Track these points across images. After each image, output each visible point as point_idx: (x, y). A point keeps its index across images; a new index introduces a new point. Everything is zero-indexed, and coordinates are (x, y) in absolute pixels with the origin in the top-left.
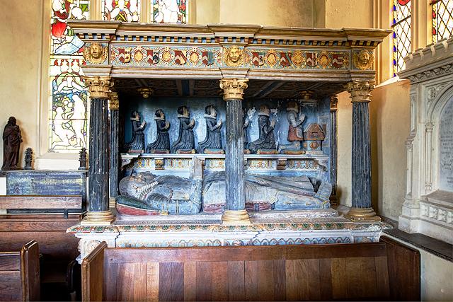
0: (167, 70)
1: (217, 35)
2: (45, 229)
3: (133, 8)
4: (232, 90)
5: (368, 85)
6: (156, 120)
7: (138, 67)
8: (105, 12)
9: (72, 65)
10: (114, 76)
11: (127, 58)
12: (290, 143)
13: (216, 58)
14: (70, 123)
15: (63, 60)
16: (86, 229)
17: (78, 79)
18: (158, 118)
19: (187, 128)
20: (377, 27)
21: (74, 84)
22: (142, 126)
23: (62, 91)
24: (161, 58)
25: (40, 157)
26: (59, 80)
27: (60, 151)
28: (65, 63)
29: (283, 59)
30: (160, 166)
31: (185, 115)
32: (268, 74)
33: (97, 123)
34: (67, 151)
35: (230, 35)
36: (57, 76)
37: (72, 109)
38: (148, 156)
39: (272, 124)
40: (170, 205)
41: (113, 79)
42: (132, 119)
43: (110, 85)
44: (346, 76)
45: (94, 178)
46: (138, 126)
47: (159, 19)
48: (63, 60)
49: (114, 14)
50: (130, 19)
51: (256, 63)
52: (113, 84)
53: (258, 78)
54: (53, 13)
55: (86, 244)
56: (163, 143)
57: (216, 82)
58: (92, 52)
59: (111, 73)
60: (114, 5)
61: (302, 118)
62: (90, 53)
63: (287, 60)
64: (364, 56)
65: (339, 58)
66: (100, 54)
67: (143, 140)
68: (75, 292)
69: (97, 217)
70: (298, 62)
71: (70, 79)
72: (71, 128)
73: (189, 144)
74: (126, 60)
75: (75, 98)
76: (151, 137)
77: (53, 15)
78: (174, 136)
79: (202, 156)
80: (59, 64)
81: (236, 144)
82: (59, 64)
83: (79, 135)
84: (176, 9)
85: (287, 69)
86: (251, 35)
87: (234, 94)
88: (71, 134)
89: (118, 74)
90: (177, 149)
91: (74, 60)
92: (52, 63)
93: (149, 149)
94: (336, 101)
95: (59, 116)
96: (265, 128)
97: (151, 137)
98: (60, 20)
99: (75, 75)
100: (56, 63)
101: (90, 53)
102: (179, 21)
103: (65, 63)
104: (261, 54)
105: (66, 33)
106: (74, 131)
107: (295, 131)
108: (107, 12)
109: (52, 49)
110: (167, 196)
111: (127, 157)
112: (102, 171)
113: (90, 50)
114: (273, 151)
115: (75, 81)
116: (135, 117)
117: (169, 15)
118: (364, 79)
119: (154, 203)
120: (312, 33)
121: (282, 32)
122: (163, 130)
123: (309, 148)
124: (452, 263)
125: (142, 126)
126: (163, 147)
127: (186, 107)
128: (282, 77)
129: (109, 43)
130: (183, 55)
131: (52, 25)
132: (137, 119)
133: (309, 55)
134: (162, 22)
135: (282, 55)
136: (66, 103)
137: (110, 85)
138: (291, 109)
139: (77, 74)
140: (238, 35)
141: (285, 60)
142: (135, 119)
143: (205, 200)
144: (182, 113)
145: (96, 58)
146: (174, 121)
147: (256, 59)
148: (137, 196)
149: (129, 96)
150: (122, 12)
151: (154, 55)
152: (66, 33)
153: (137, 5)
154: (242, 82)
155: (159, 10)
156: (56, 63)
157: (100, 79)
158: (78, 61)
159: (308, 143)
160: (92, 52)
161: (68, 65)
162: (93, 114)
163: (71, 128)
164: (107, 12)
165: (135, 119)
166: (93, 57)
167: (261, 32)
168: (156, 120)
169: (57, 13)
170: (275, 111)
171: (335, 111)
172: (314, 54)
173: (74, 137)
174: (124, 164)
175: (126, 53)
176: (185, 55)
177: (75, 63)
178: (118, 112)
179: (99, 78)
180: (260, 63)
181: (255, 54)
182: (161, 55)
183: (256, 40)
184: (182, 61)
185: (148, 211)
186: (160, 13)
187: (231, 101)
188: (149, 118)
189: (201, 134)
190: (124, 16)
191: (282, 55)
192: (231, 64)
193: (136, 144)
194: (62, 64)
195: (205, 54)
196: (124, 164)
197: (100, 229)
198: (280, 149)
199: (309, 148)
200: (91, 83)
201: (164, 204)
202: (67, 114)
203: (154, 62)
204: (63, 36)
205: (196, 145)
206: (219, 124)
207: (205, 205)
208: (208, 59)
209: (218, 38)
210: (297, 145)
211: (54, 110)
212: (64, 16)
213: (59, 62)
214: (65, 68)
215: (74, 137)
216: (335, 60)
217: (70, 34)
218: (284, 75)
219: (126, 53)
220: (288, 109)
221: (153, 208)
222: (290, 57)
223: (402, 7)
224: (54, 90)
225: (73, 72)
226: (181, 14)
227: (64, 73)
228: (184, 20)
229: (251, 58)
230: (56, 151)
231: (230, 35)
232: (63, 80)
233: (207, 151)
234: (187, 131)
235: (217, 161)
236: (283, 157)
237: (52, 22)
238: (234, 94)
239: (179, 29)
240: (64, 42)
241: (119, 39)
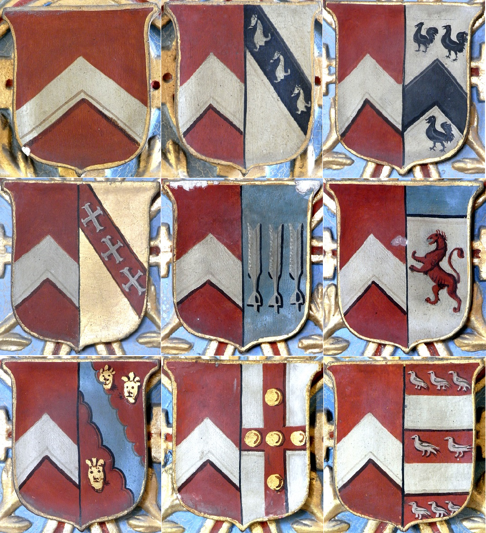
29: (49, 440)
130: (107, 234)
141: (66, 455)
151: (417, 63)
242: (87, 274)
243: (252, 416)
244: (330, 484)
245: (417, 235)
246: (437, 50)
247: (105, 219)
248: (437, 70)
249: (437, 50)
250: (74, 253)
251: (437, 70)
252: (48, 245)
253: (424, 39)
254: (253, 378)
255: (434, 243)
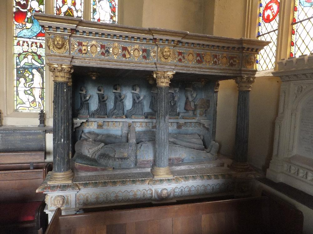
0: (115, 60)
1: (155, 37)
2: (15, 179)
3: (78, 6)
4: (163, 80)
5: (252, 79)
6: (98, 94)
7: (91, 55)
8: (57, 7)
9: (32, 46)
10: (73, 64)
11: (85, 50)
12: (185, 111)
13: (152, 54)
14: (31, 90)
15: (24, 42)
16: (53, 188)
17: (36, 58)
18: (99, 92)
19: (119, 100)
20: (247, 37)
21: (34, 62)
22: (88, 98)
23: (24, 66)
24: (111, 51)
25: (8, 116)
26: (22, 56)
27: (24, 111)
28: (25, 44)
29: (198, 58)
30: (100, 126)
31: (118, 91)
32: (188, 69)
33: (60, 103)
34: (29, 111)
35: (164, 38)
36: (20, 54)
37: (32, 80)
38: (92, 120)
39: (176, 99)
40: (115, 163)
41: (74, 67)
42: (81, 92)
43: (70, 71)
44: (238, 72)
45: (58, 147)
46: (85, 98)
47: (97, 17)
48: (24, 42)
49: (64, 9)
50: (75, 14)
51: (180, 60)
52: (72, 71)
53: (181, 71)
54: (15, 3)
55: (53, 199)
56: (103, 112)
57: (150, 73)
58: (56, 43)
59: (71, 62)
60: (64, 2)
61: (194, 95)
62: (54, 44)
63: (200, 59)
64: (251, 59)
65: (234, 59)
66: (63, 45)
67: (88, 108)
68: (41, 229)
69: (60, 177)
70: (208, 60)
71: (30, 57)
72: (31, 94)
73: (121, 111)
74: (83, 52)
75: (34, 71)
76: (94, 105)
77: (15, 5)
78: (110, 105)
79: (129, 121)
80: (21, 45)
81: (165, 120)
82: (21, 45)
83: (38, 100)
84: (109, 10)
85: (200, 65)
86: (180, 39)
87: (164, 83)
88: (31, 99)
89: (77, 63)
90: (113, 114)
91: (33, 43)
92: (15, 44)
93: (93, 115)
94: (218, 85)
95: (22, 85)
96: (172, 102)
97: (94, 105)
98: (21, 10)
99: (34, 54)
100: (18, 44)
101: (54, 44)
102: (111, 20)
103: (25, 44)
104: (183, 53)
105: (26, 20)
106: (34, 96)
107: (190, 103)
108: (58, 7)
109: (16, 32)
110: (112, 155)
111: (78, 121)
112: (64, 141)
113: (54, 42)
114: (177, 117)
115: (34, 59)
116: (82, 91)
117: (104, 14)
118: (249, 75)
119: (103, 162)
120: (202, 38)
121: (177, 35)
122: (102, 100)
123: (198, 115)
124: (312, 210)
125: (88, 98)
126: (102, 113)
127: (119, 85)
128: (197, 71)
129: (70, 36)
130: (128, 51)
131: (15, 13)
132: (84, 92)
133: (215, 56)
134: (99, 20)
135: (198, 55)
136: (27, 75)
137: (70, 71)
138: (189, 89)
139: (36, 53)
140: (170, 38)
141: (199, 59)
142: (82, 92)
143: (138, 157)
144: (116, 89)
145: (60, 48)
146: (110, 95)
147: (180, 57)
148: (89, 155)
149: (80, 77)
150: (70, 9)
151: (106, 49)
152: (26, 20)
153: (81, 4)
154: (170, 74)
155: (97, 10)
156: (18, 44)
157: (63, 66)
158: (36, 43)
159: (198, 112)
160: (56, 43)
161: (28, 46)
162: (56, 95)
163: (31, 94)
164: (58, 7)
165: (82, 92)
166: (56, 47)
167: (187, 37)
168: (98, 94)
169: (18, 4)
170: (177, 90)
171: (217, 92)
172: (219, 56)
173: (34, 101)
174: (75, 126)
175: (84, 45)
176: (130, 50)
177: (34, 45)
178: (71, 88)
179: (61, 65)
180: (183, 60)
181: (180, 54)
182: (111, 49)
183: (182, 42)
184: (128, 56)
185: (98, 168)
186: (98, 12)
187: (162, 88)
188: (92, 94)
189: (128, 104)
190: (71, 12)
191: (198, 55)
192: (163, 59)
193: (83, 111)
194: (23, 45)
195: (144, 51)
196: (75, 126)
197: (64, 187)
198: (180, 116)
199: (198, 115)
200: (54, 69)
201: (111, 162)
202: (28, 84)
203: (106, 54)
204: (24, 23)
205: (125, 112)
206: (142, 98)
207: (138, 161)
208: (146, 54)
209: (156, 39)
210: (191, 113)
211: (18, 80)
212: (24, 6)
213: (21, 43)
214: (25, 48)
215: (34, 101)
216: (232, 61)
217: (29, 22)
218: (198, 70)
219: (84, 45)
220: (187, 89)
221: (103, 166)
222: (203, 57)
223: (267, 24)
224: (17, 65)
225: (32, 52)
226: (112, 15)
227: (25, 52)
228: (114, 19)
229: (177, 56)
230: (20, 111)
231: (164, 38)
232: (24, 57)
233: (133, 116)
234: (120, 102)
235: (138, 123)
236: (182, 121)
237: (14, 10)
238: (164, 83)
239: (127, 30)
240: (25, 27)
241: (78, 33)
242: (127, 53)
243: (218, 58)
244: (2, 114)
245: (183, 55)
246: (107, 48)
247: (128, 49)
248: (107, 50)
249: (107, 48)
250: (126, 51)
251: (107, 50)
252: (124, 51)
253: (106, 47)
254: (218, 56)
255: (291, 48)
